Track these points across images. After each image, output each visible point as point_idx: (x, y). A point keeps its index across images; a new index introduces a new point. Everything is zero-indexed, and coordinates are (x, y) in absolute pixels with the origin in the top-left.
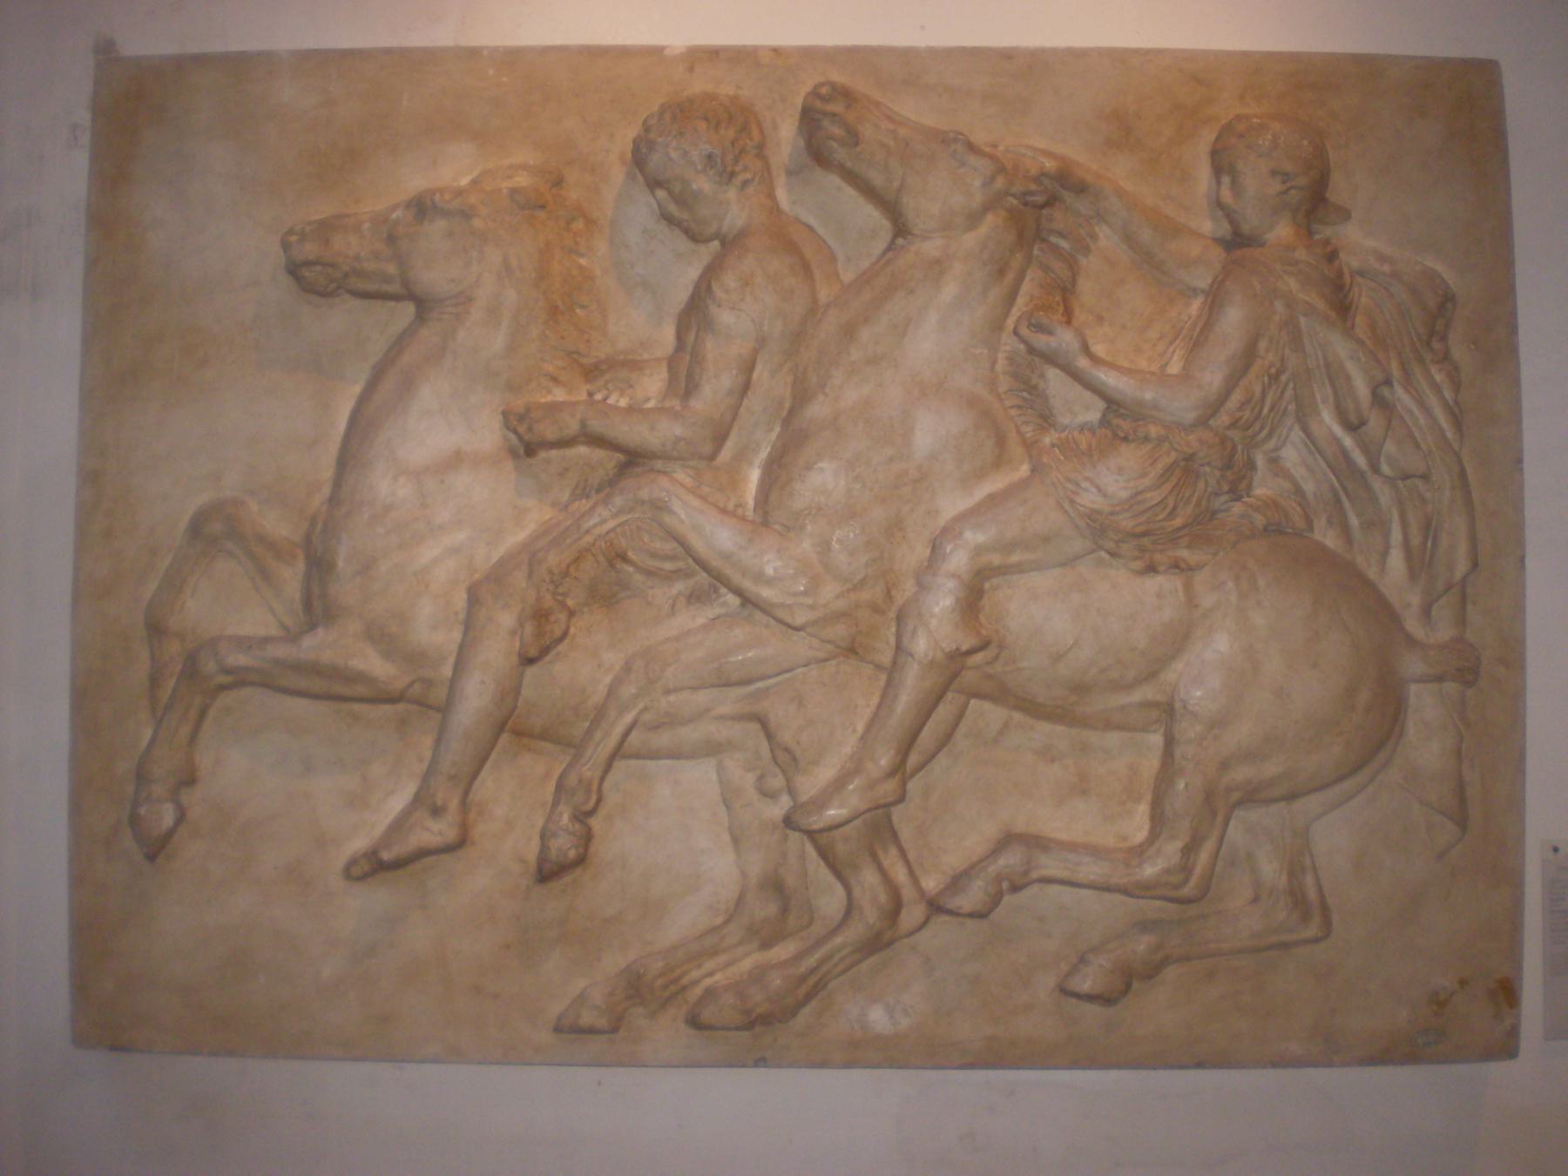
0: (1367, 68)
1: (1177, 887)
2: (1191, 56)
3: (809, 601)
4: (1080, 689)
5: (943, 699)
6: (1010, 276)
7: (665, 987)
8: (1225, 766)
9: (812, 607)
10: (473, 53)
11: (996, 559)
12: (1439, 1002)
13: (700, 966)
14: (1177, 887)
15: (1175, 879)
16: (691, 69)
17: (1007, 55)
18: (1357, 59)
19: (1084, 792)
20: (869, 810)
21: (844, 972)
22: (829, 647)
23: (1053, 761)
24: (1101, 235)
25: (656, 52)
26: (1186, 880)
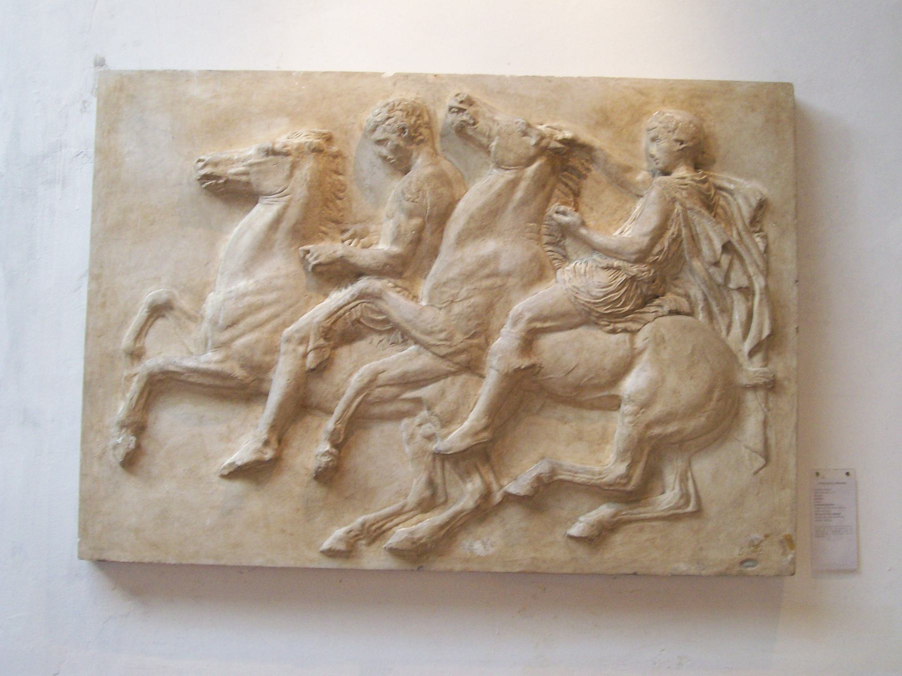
0: (726, 88)
1: (625, 485)
2: (640, 81)
3: (449, 343)
4: (579, 388)
5: (239, 565)
6: (548, 188)
7: (375, 531)
8: (649, 426)
9: (450, 346)
10: (289, 74)
11: (539, 325)
12: (755, 546)
13: (392, 520)
14: (625, 485)
15: (624, 481)
16: (395, 84)
17: (549, 80)
18: (722, 83)
19: (580, 439)
20: (391, 528)
21: (615, 279)
22: (457, 367)
23: (565, 423)
24: (593, 169)
25: (376, 75)
26: (628, 483)
